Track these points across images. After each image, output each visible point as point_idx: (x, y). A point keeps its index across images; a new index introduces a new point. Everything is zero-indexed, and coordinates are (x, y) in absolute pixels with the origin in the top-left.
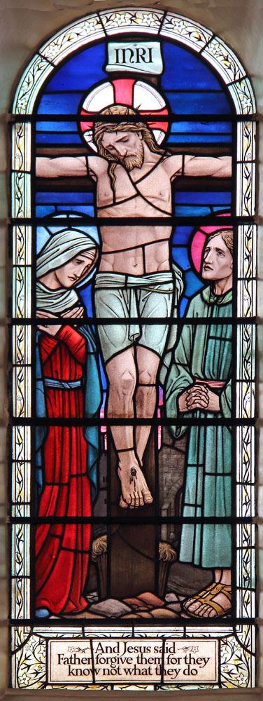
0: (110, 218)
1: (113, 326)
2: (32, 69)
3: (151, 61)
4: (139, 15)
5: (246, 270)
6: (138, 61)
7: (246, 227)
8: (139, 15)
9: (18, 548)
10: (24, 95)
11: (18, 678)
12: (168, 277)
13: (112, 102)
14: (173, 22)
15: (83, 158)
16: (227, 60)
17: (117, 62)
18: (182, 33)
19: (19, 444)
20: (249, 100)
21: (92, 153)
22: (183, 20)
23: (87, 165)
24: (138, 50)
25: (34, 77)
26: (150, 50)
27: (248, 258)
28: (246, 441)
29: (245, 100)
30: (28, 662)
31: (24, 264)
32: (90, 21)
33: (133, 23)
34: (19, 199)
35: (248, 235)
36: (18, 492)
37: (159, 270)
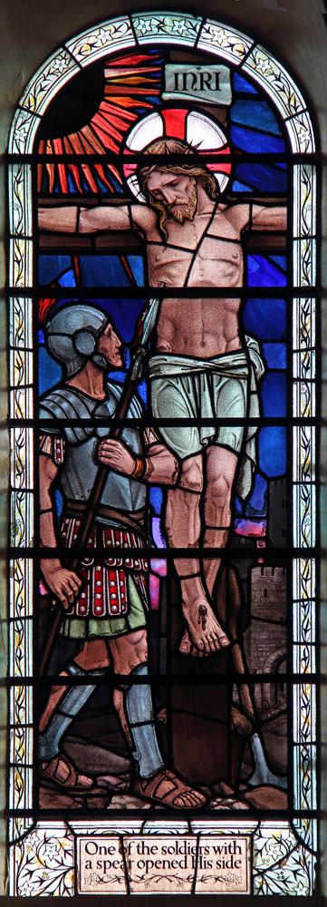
0: (258, 288)
1: (182, 428)
2: (33, 89)
3: (218, 88)
6: (202, 89)
7: (303, 301)
10: (22, 124)
11: (18, 888)
12: (239, 359)
13: (161, 134)
14: (211, 31)
15: (126, 208)
16: (278, 80)
17: (176, 88)
18: (223, 45)
19: (19, 581)
20: (308, 132)
21: (136, 202)
23: (130, 216)
24: (202, 75)
26: (217, 74)
28: (305, 577)
30: (30, 867)
31: (23, 346)
32: (105, 28)
33: (161, 32)
37: (230, 350)
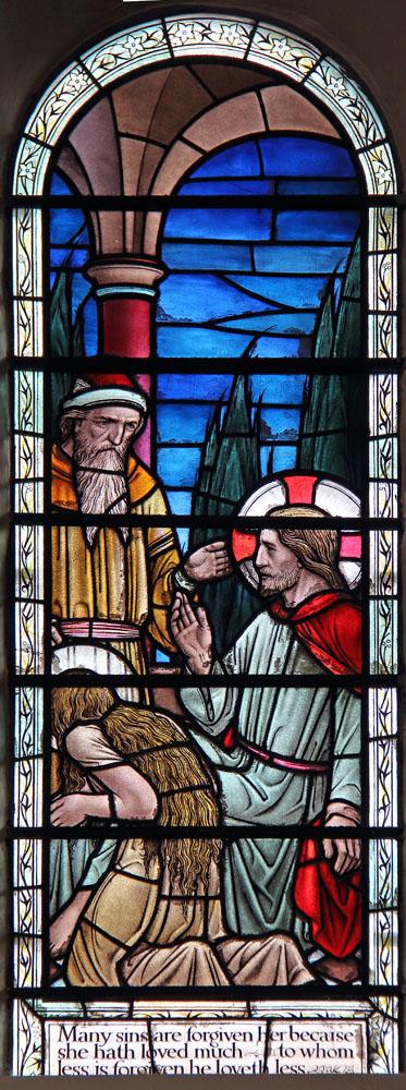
4: (215, 26)
5: (381, 509)
7: (381, 378)
8: (215, 26)
9: (23, 878)
10: (30, 156)
16: (354, 105)
18: (285, 58)
22: (287, 37)
25: (45, 125)
27: (385, 865)
29: (382, 171)
32: (135, 35)
34: (24, 326)
35: (385, 388)
36: (23, 790)
